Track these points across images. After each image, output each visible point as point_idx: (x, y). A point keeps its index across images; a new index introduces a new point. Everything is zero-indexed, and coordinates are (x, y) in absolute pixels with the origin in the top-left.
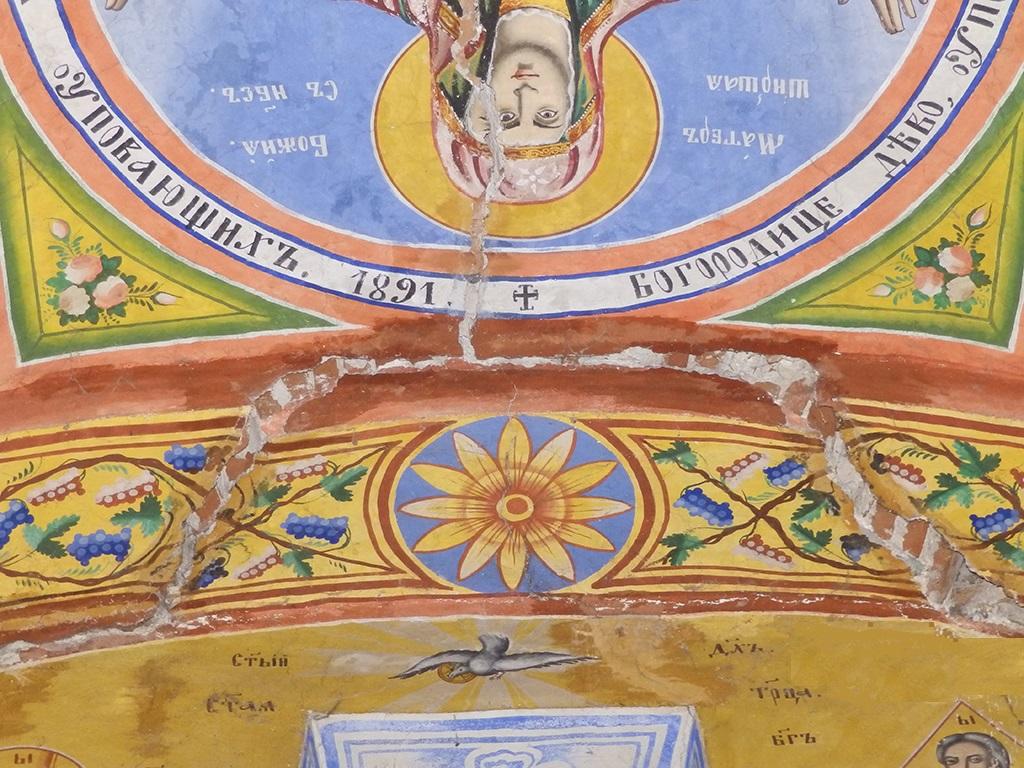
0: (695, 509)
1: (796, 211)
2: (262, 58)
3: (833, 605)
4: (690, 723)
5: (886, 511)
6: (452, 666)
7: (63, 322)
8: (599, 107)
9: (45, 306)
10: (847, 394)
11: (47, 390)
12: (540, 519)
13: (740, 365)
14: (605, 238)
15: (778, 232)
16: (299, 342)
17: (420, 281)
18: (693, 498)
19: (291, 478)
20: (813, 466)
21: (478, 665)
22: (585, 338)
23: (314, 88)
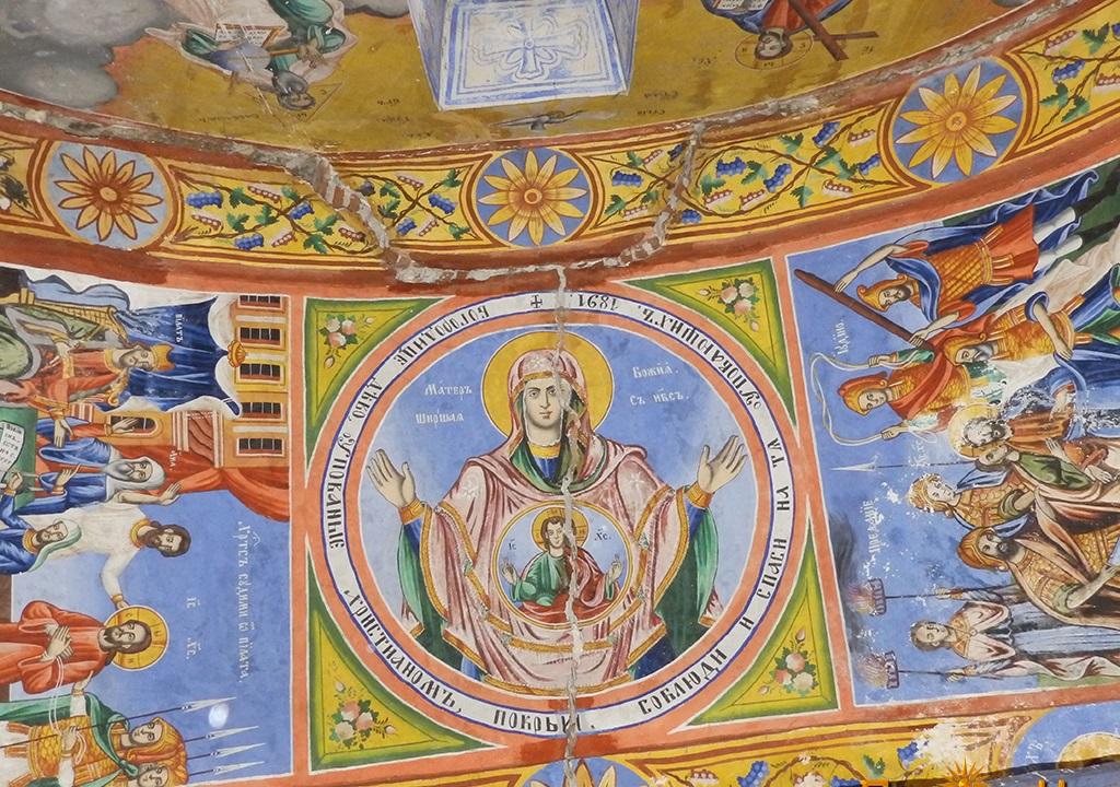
0: (447, 202)
1: (416, 356)
2: (666, 415)
3: (376, 156)
4: (440, 101)
6: (558, 117)
7: (751, 279)
8: (511, 399)
9: (760, 287)
10: (381, 271)
11: (757, 245)
12: (521, 191)
13: (431, 275)
14: (502, 335)
15: (423, 345)
16: (640, 272)
17: (586, 306)
18: (449, 208)
19: (641, 207)
20: (393, 231)
21: (547, 118)
22: (508, 282)
23: (641, 401)
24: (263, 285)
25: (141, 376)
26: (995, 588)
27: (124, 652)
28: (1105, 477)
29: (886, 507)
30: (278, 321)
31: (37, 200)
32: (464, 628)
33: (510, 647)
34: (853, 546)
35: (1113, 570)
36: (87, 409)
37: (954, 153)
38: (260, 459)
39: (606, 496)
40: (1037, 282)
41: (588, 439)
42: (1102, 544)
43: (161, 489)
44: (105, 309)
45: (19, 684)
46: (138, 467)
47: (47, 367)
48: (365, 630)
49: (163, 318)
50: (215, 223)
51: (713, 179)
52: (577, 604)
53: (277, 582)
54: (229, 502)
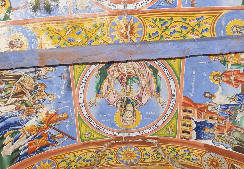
1: (155, 125)
2: (104, 112)
3: (160, 165)
5: (165, 155)
7: (85, 138)
8: (136, 116)
11: (84, 145)
12: (131, 157)
13: (150, 141)
15: (153, 127)
17: (119, 133)
19: (107, 153)
20: (158, 150)
22: (135, 138)
24: (184, 141)
25: (211, 127)
26: (39, 80)
27: (219, 75)
28: (16, 103)
29: (60, 94)
30: (182, 134)
31: (229, 165)
32: (148, 72)
33: (139, 68)
34: (67, 87)
35: (15, 85)
36: (222, 122)
37: (44, 165)
38: (188, 108)
39: (117, 97)
40: (28, 141)
41: (120, 108)
42: (17, 90)
43: (209, 105)
44: (217, 141)
45: (241, 72)
46: (213, 110)
47: (230, 132)
48: (169, 73)
49: (205, 138)
50: (194, 155)
51: (92, 158)
52: (125, 76)
53: (186, 84)
54: (195, 101)
